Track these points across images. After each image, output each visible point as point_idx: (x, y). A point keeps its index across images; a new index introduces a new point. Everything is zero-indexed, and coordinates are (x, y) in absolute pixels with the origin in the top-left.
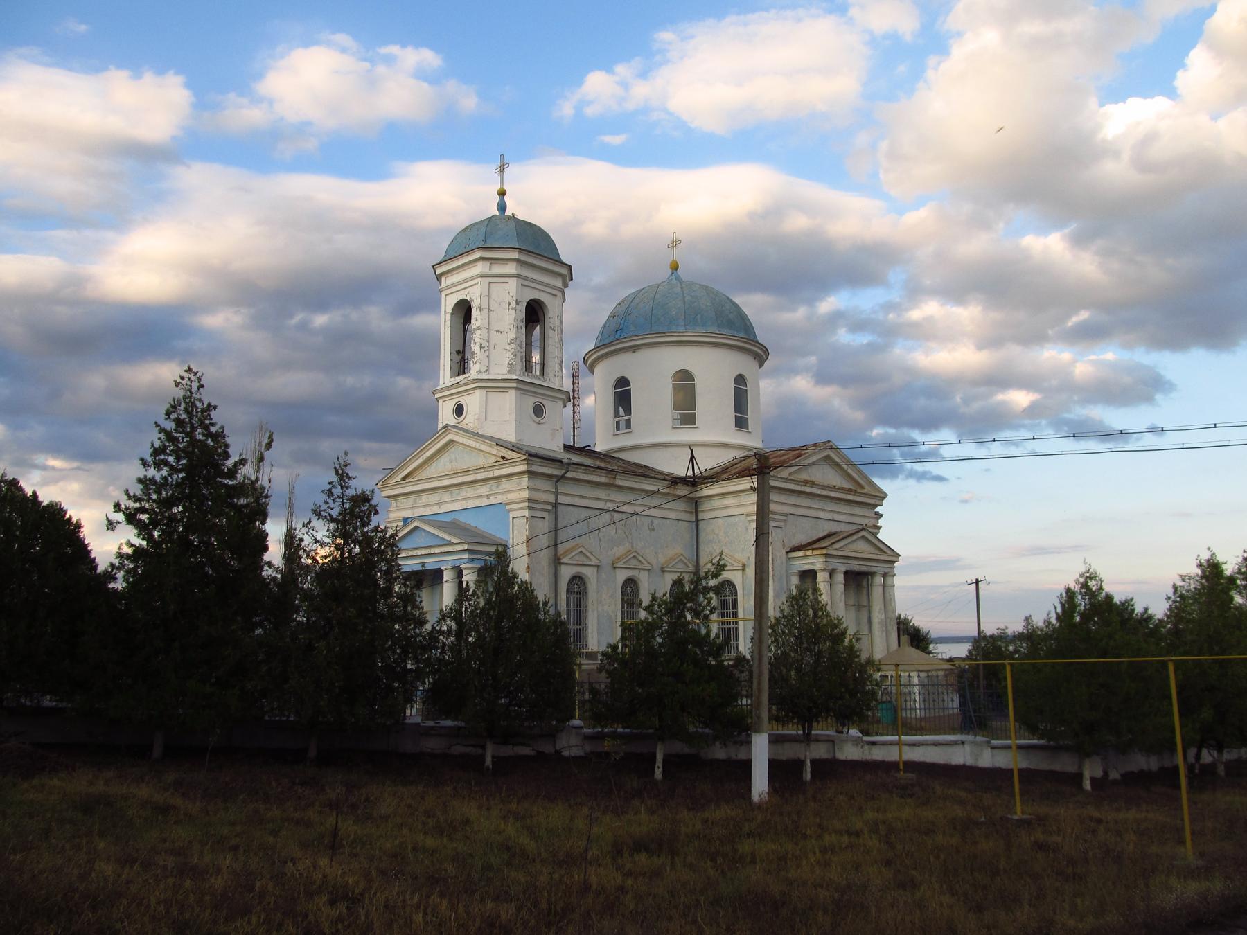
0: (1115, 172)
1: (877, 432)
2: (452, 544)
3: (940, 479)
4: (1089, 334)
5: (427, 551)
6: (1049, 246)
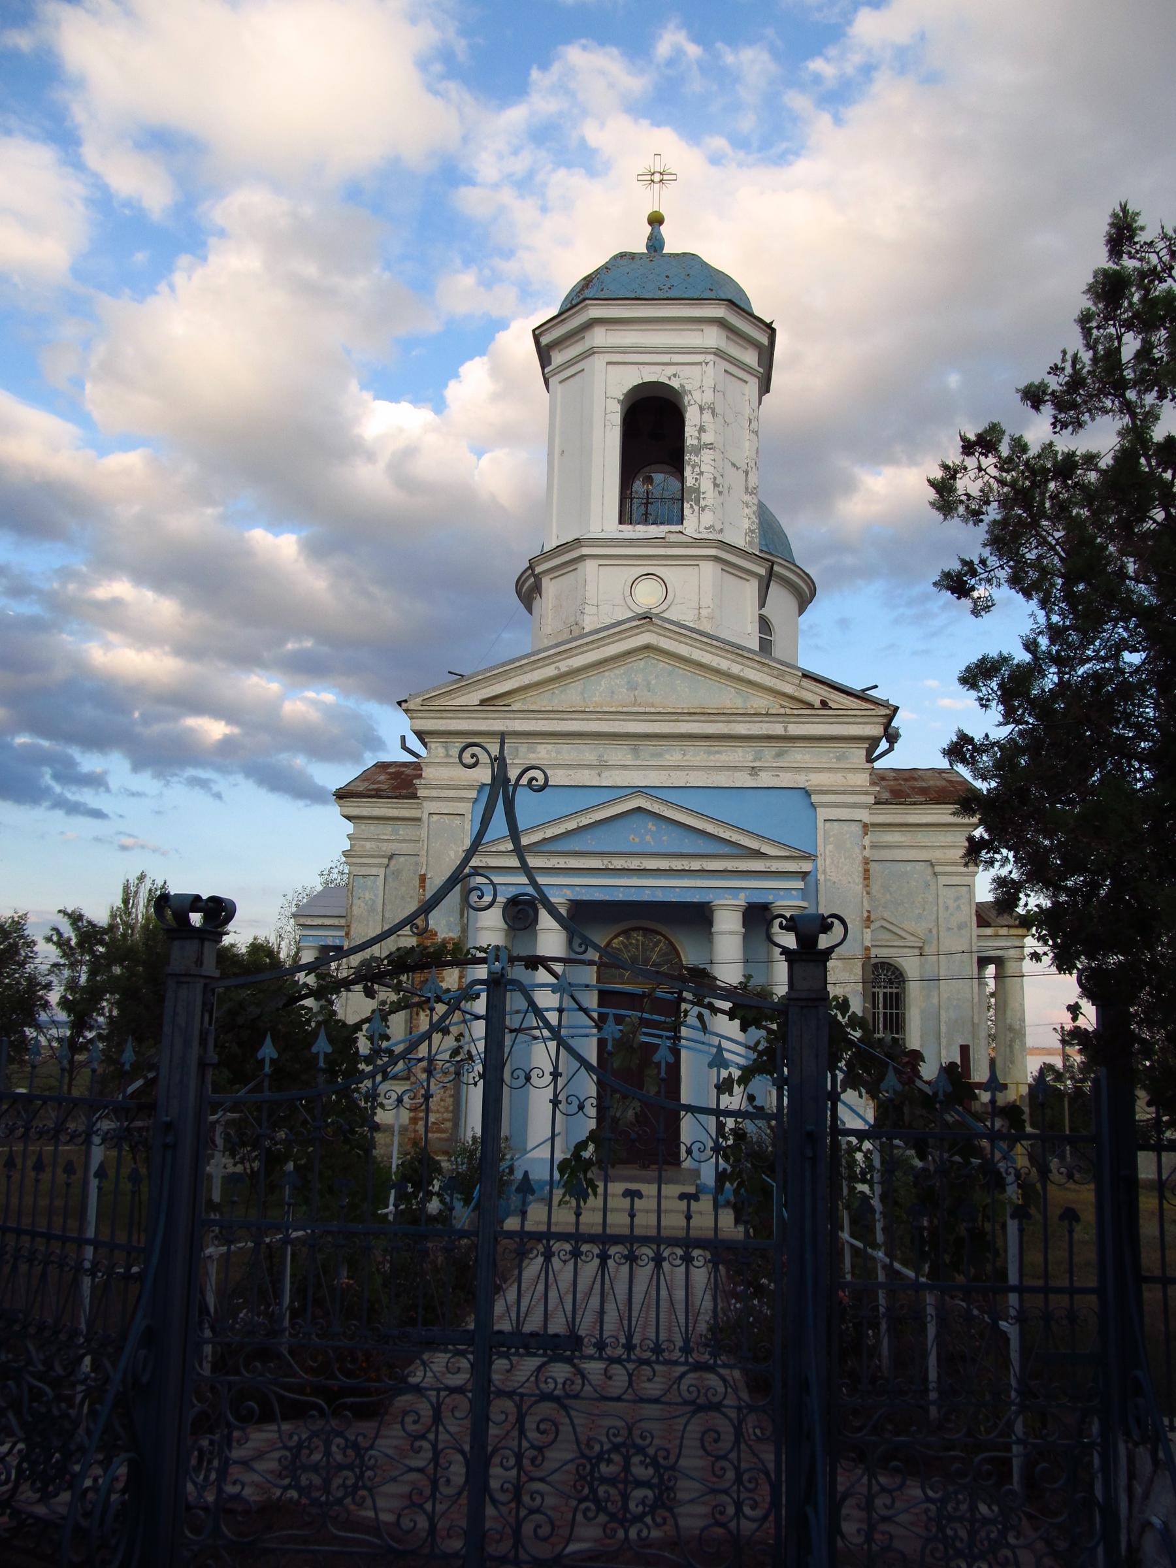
0: (370, 479)
1: (22, 739)
2: (758, 855)
3: (98, 814)
4: (307, 668)
5: (677, 864)
6: (280, 546)
